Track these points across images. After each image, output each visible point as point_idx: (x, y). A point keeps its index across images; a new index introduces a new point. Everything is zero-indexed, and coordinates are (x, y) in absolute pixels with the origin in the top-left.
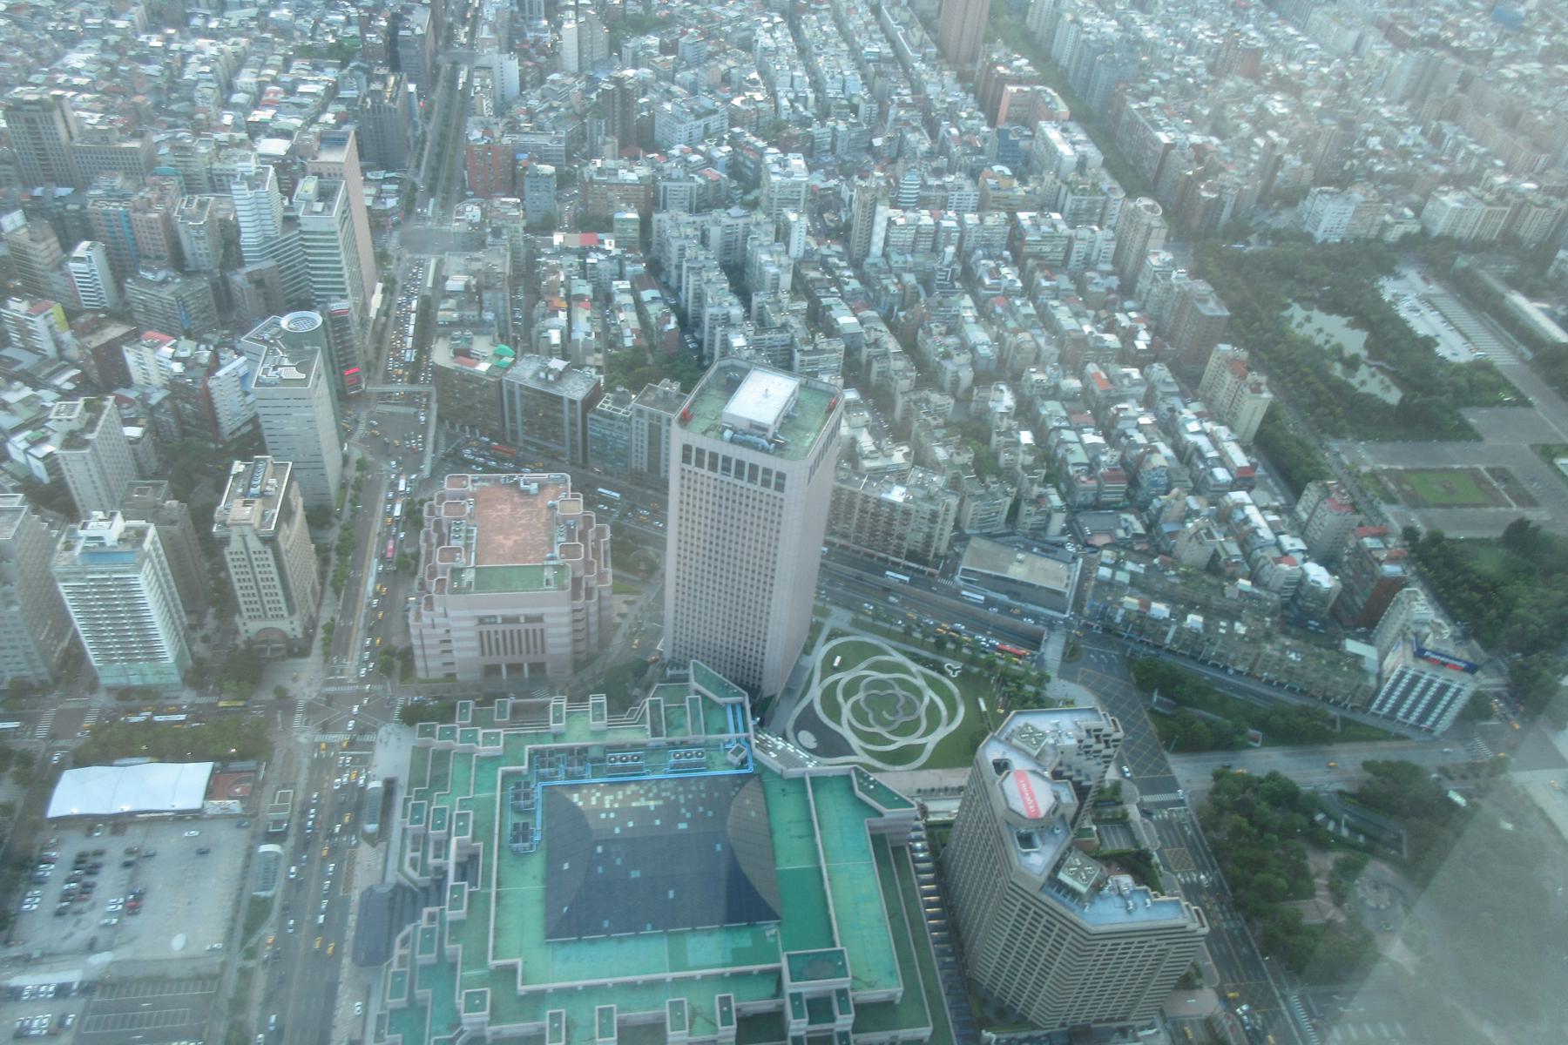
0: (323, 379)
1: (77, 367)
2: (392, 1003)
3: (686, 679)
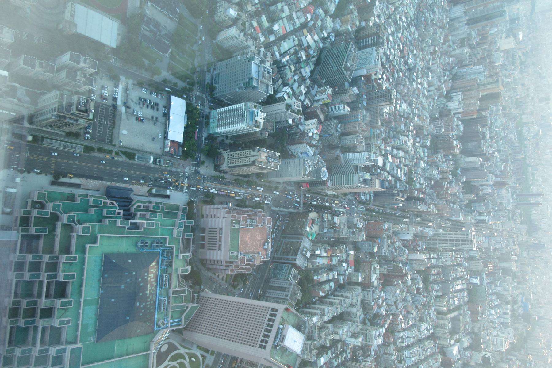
2: (91, 200)
3: (193, 302)
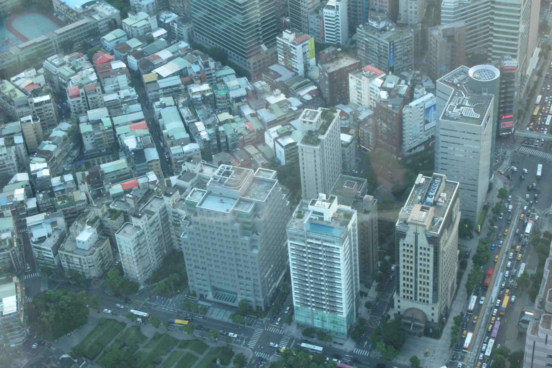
1: (315, 84)
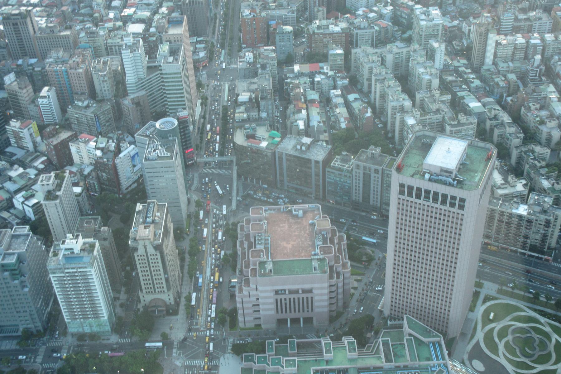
0: (179, 155)
1: (45, 155)
3: (401, 326)
